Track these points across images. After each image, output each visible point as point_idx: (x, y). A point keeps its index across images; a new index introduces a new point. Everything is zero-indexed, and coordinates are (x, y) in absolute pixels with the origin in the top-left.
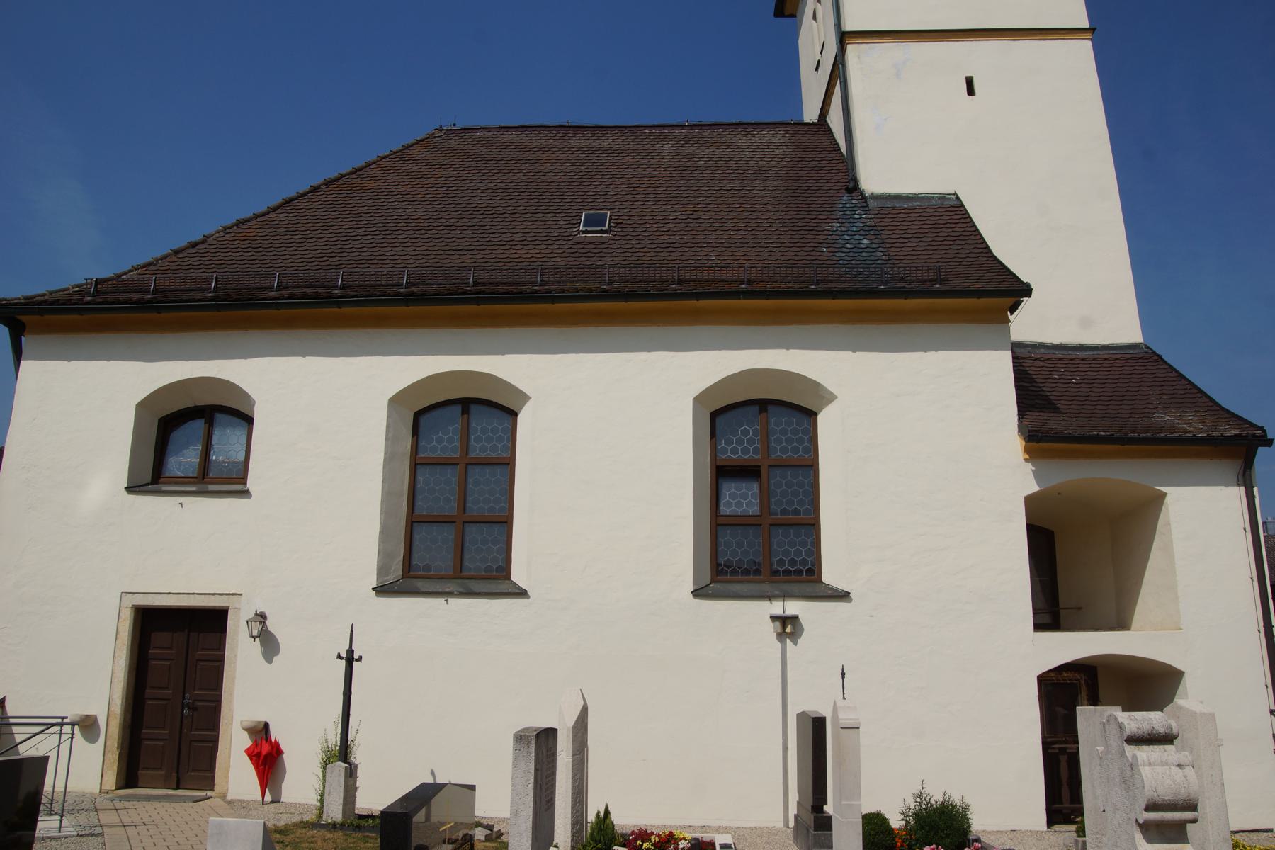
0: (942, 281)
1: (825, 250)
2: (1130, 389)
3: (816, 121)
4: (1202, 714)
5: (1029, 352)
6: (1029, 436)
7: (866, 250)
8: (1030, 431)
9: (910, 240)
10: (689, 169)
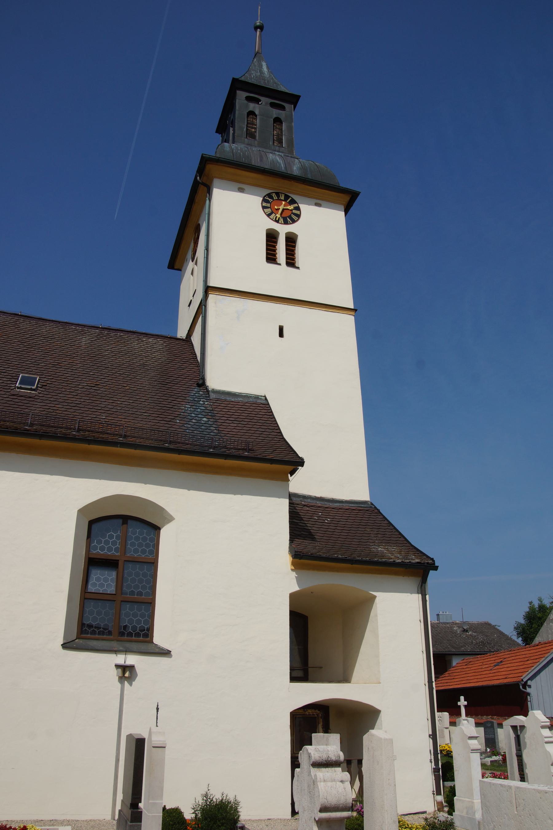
0: (250, 450)
1: (178, 421)
2: (359, 529)
3: (185, 338)
4: (386, 740)
5: (301, 501)
6: (295, 554)
7: (205, 425)
8: (295, 552)
9: (233, 422)
10: (97, 356)
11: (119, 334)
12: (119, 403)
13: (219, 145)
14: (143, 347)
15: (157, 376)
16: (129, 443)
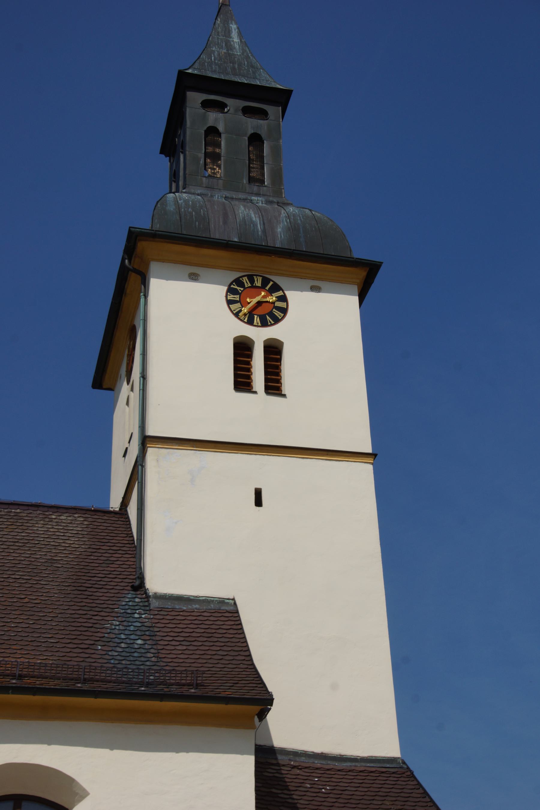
0: (197, 686)
1: (100, 647)
3: (118, 509)
7: (138, 651)
11: (13, 510)
12: (13, 625)
13: (158, 202)
14: (51, 530)
15: (72, 577)
16: (25, 687)
